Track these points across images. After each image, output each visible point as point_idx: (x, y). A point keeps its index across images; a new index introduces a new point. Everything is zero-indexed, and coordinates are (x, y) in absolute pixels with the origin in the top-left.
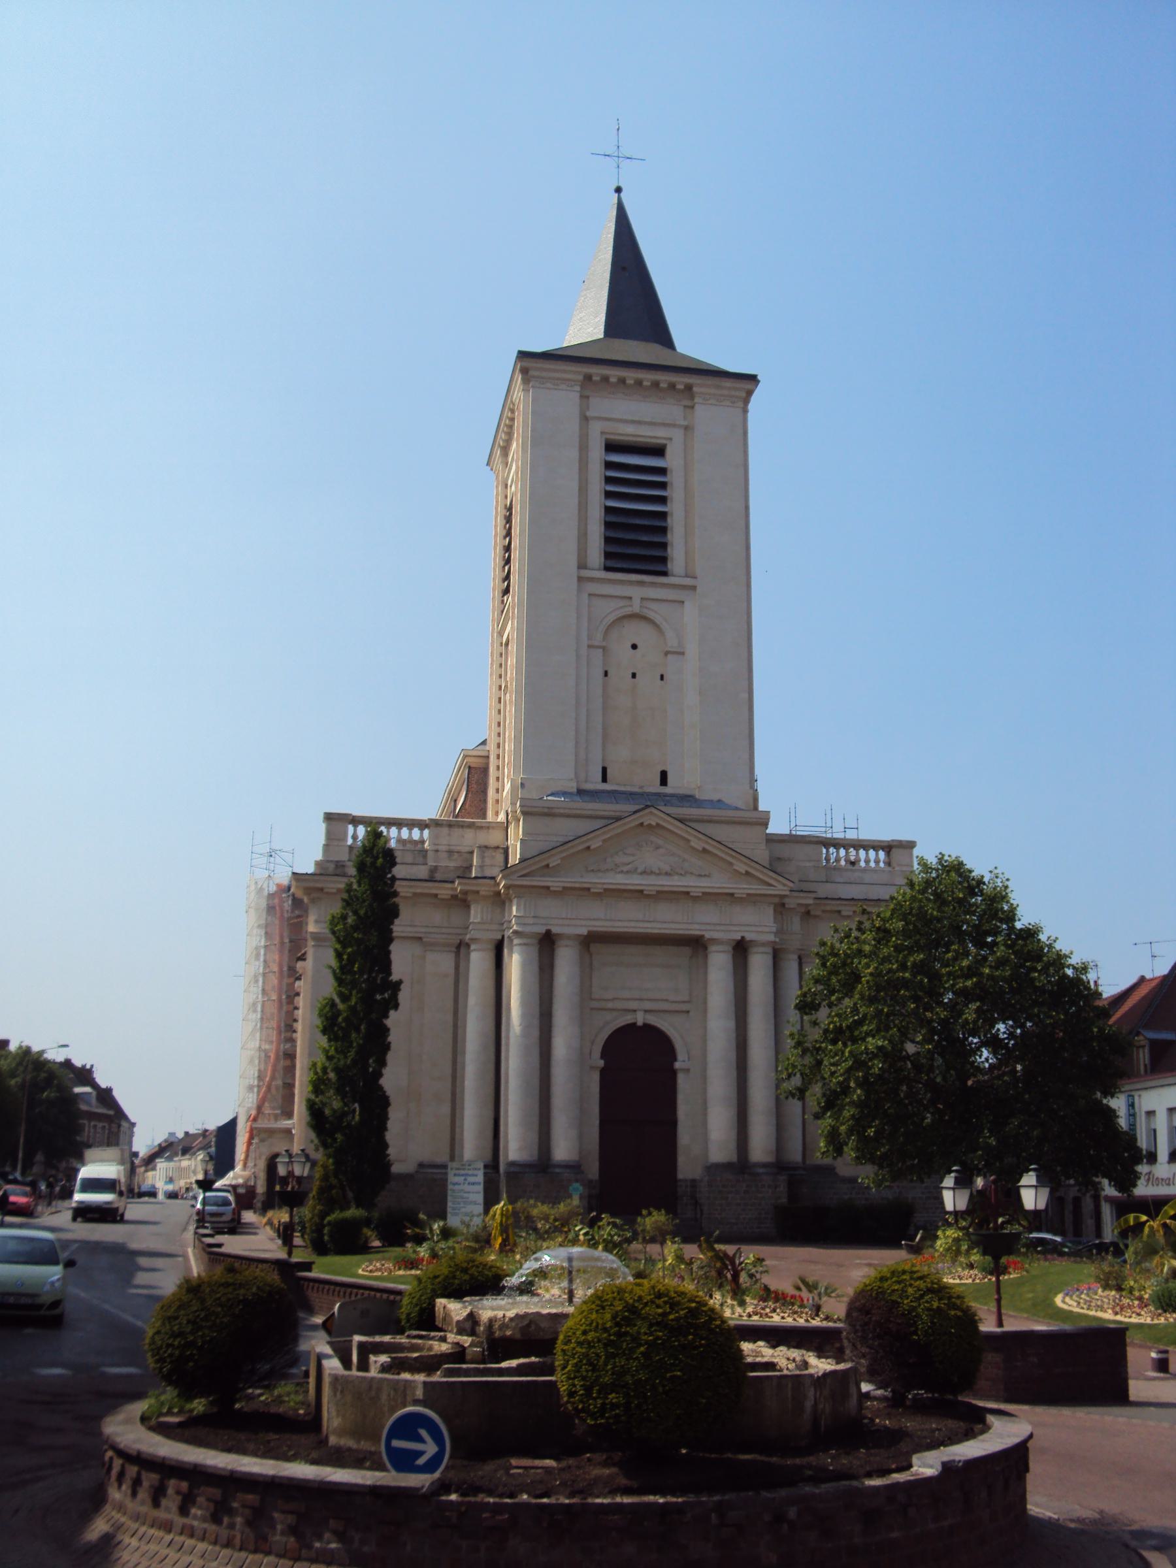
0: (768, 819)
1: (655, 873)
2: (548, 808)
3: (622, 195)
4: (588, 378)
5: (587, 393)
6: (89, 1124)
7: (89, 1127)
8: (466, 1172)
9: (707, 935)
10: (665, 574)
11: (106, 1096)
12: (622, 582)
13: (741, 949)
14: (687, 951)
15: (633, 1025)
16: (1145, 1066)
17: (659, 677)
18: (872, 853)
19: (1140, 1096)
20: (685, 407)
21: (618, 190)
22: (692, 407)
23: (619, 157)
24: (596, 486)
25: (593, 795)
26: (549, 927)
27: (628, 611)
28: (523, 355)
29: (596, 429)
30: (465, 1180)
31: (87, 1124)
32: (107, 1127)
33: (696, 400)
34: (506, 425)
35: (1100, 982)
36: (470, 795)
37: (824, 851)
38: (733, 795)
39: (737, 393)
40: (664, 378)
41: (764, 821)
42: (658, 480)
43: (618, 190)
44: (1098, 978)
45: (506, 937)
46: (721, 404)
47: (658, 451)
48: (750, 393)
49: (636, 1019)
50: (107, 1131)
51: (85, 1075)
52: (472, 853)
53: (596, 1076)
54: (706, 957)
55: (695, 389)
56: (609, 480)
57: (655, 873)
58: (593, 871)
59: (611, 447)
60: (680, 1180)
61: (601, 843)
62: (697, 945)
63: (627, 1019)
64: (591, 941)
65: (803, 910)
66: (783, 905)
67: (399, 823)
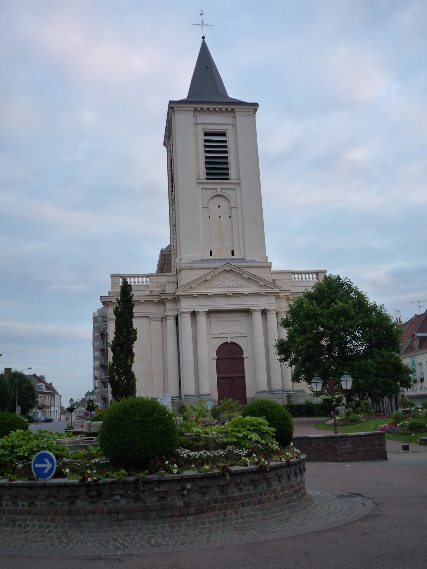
0: (271, 265)
1: (231, 287)
2: (191, 266)
3: (205, 39)
4: (196, 109)
5: (195, 115)
6: (43, 396)
7: (43, 397)
8: (165, 398)
9: (252, 308)
10: (228, 179)
11: (49, 387)
12: (213, 183)
13: (264, 312)
14: (245, 315)
15: (227, 343)
16: (417, 347)
17: (229, 217)
18: (311, 275)
19: (416, 357)
20: (232, 117)
21: (203, 38)
22: (235, 117)
23: (202, 25)
24: (202, 149)
25: (207, 261)
26: (194, 309)
27: (215, 194)
28: (171, 102)
29: (200, 127)
30: (165, 401)
31: (42, 396)
32: (50, 397)
33: (236, 114)
34: (168, 129)
35: (401, 318)
36: (165, 265)
37: (293, 275)
38: (258, 258)
39: (190, 109)
40: (224, 107)
41: (270, 267)
42: (223, 145)
43: (203, 38)
44: (401, 316)
45: (179, 314)
46: (190, 113)
47: (223, 134)
48: (256, 110)
49: (228, 340)
50: (50, 399)
51: (41, 379)
52: (165, 285)
53: (215, 362)
54: (252, 316)
55: (235, 110)
56: (206, 146)
57: (231, 287)
58: (208, 288)
59: (206, 134)
60: (248, 398)
61: (211, 278)
62: (248, 312)
63: (225, 341)
64: (210, 313)
65: (286, 297)
66: (288, 298)
67: (134, 276)
